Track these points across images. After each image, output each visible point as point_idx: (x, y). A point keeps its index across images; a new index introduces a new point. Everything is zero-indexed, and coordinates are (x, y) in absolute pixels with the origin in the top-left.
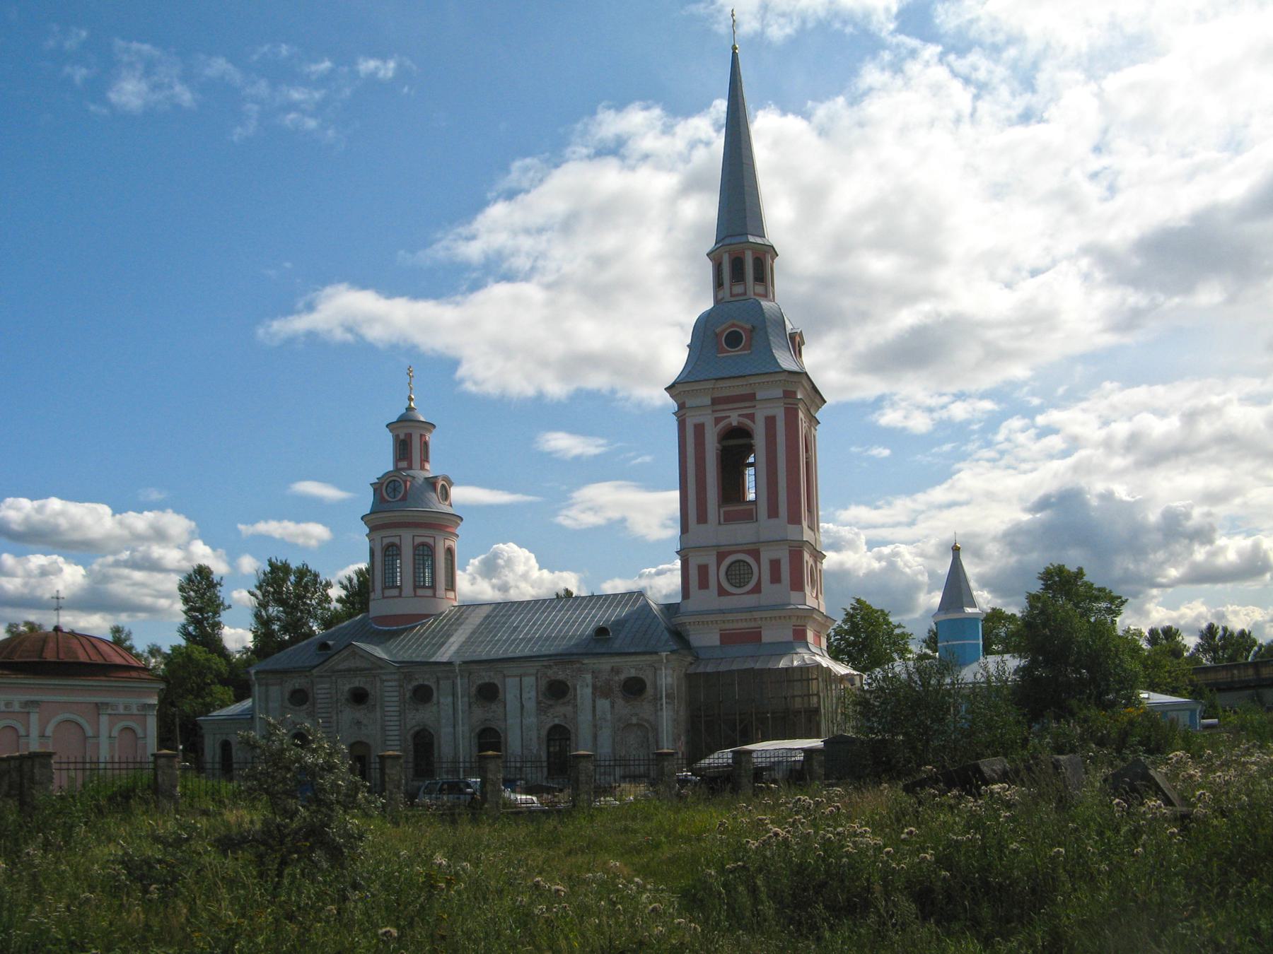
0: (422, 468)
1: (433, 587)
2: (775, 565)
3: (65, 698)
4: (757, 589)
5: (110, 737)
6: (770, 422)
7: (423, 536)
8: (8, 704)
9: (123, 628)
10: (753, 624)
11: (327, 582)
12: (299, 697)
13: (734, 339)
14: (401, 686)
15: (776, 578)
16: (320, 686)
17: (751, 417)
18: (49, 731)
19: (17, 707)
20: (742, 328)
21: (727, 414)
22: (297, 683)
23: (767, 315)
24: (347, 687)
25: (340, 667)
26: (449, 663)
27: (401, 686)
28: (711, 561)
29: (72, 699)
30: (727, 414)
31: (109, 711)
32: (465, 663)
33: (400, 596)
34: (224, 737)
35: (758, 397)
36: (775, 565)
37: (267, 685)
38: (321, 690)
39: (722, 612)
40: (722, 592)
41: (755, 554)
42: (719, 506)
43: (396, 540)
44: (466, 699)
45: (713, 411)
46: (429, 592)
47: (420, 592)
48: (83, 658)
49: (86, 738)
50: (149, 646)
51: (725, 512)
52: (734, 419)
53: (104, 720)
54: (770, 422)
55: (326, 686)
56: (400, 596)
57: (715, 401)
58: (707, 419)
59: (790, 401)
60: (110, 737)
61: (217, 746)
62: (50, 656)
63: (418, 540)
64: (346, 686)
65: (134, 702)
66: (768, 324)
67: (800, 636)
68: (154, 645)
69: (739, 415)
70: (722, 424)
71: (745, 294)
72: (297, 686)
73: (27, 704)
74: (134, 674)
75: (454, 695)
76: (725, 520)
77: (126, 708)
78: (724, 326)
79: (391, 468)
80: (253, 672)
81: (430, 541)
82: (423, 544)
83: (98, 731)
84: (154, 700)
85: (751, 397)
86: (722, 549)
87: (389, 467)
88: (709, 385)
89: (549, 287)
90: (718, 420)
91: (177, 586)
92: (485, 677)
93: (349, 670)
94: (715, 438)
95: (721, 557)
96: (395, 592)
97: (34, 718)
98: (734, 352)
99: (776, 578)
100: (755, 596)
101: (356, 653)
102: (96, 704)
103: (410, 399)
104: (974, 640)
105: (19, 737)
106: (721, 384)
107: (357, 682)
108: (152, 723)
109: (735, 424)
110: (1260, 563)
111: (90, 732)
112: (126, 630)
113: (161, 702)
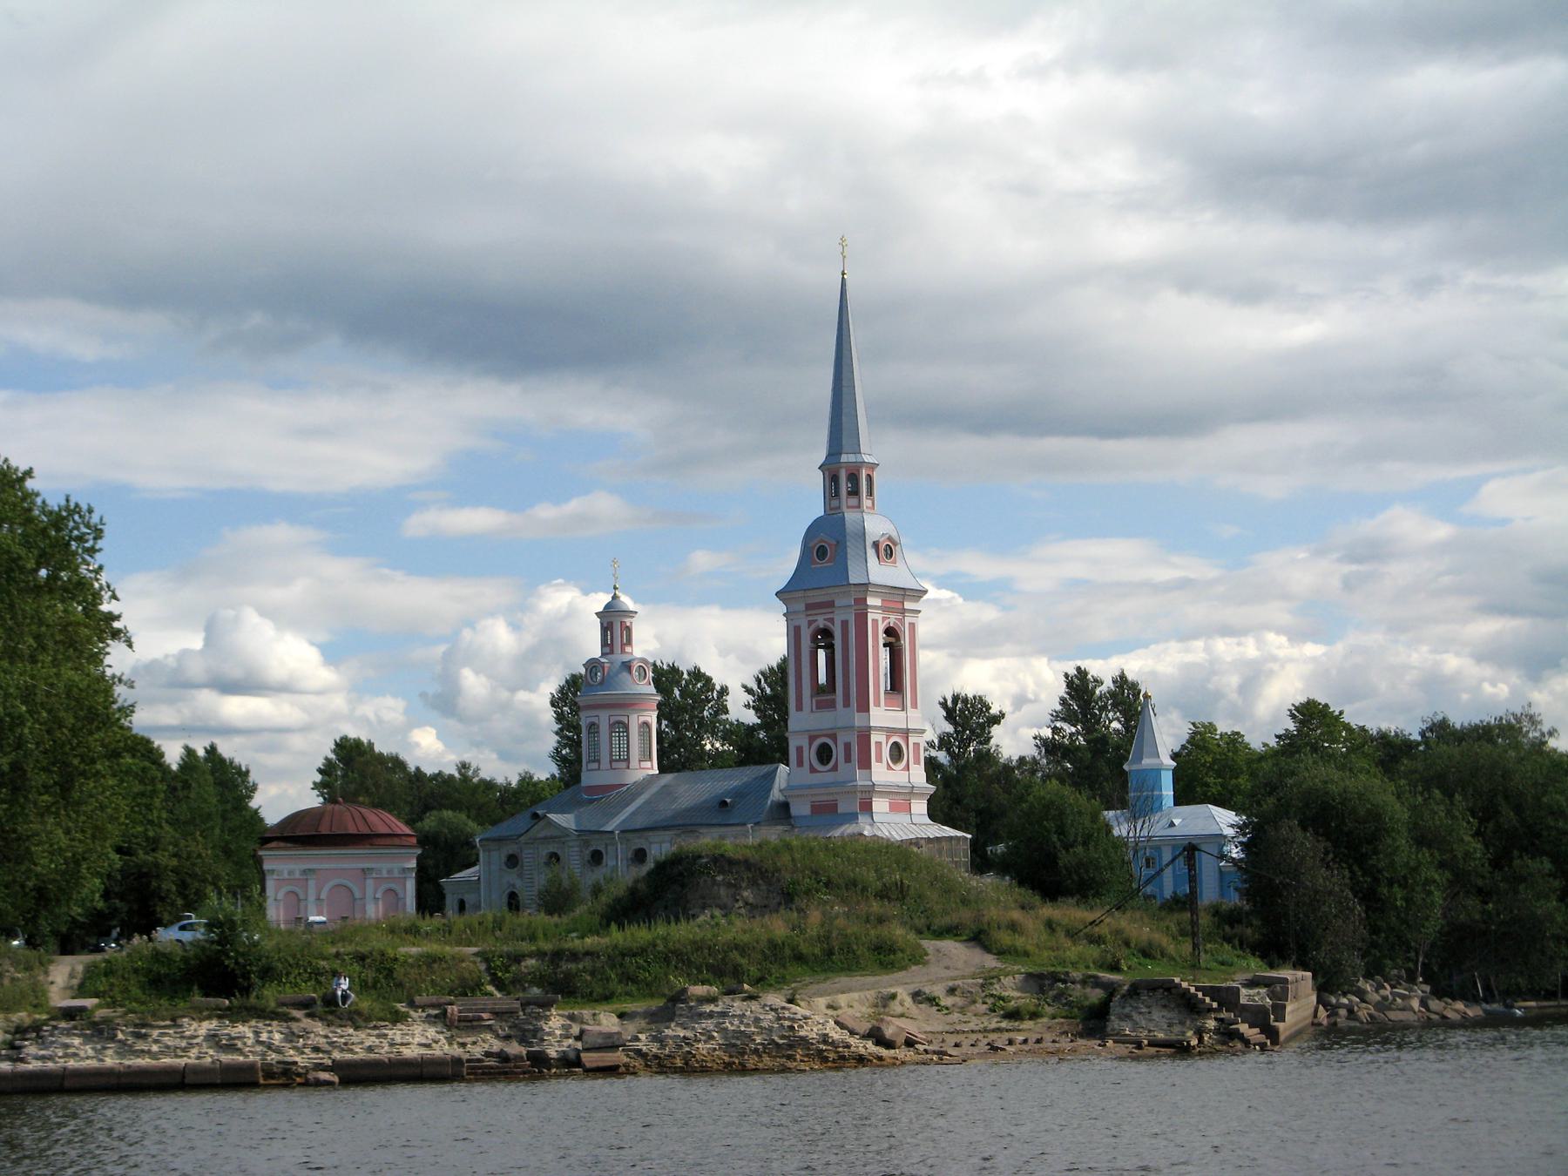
0: (623, 651)
1: (628, 760)
2: (848, 747)
3: (333, 866)
4: (835, 768)
5: (276, 900)
6: (845, 624)
7: (618, 715)
8: (290, 873)
9: (470, 764)
10: (831, 798)
11: (722, 688)
12: (512, 861)
13: (822, 552)
14: (581, 851)
15: (848, 759)
16: (526, 852)
17: (832, 620)
18: (323, 896)
19: (297, 875)
20: (829, 545)
21: (815, 618)
22: (511, 848)
23: (848, 531)
24: (546, 851)
25: (540, 835)
26: (612, 832)
27: (581, 851)
28: (805, 744)
29: (340, 866)
30: (815, 618)
31: (374, 875)
32: (623, 832)
33: (599, 769)
34: (460, 897)
35: (836, 604)
36: (848, 747)
37: (489, 851)
38: (527, 857)
39: (810, 787)
40: (813, 770)
41: (834, 737)
42: (812, 697)
43: (595, 720)
44: (625, 862)
45: (807, 615)
46: (624, 765)
47: (615, 765)
48: (352, 830)
49: (355, 899)
50: (520, 774)
51: (817, 701)
52: (821, 622)
53: (370, 883)
54: (845, 624)
55: (531, 851)
56: (599, 769)
57: (809, 607)
58: (803, 623)
59: (862, 607)
60: (276, 900)
61: (456, 902)
62: (324, 830)
63: (613, 719)
64: (545, 851)
65: (396, 866)
66: (848, 537)
67: (867, 807)
68: (526, 773)
69: (825, 620)
70: (813, 626)
71: (839, 507)
72: (511, 852)
73: (305, 872)
74: (396, 841)
75: (617, 858)
76: (818, 708)
77: (389, 872)
78: (816, 541)
79: (823, 514)
80: (477, 840)
81: (622, 719)
82: (619, 722)
83: (365, 894)
84: (413, 864)
85: (831, 604)
86: (812, 733)
87: (819, 511)
88: (800, 594)
89: (236, 863)
90: (810, 623)
91: (549, 700)
92: (639, 843)
93: (545, 838)
94: (809, 638)
95: (812, 739)
96: (595, 766)
97: (312, 883)
98: (824, 564)
99: (848, 759)
100: (832, 774)
101: (551, 823)
102: (363, 870)
103: (615, 588)
104: (1157, 785)
105: (299, 900)
106: (810, 593)
107: (552, 848)
108: (411, 886)
109: (821, 626)
110: (1465, 697)
111: (357, 895)
112: (474, 766)
113: (418, 864)
